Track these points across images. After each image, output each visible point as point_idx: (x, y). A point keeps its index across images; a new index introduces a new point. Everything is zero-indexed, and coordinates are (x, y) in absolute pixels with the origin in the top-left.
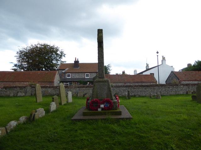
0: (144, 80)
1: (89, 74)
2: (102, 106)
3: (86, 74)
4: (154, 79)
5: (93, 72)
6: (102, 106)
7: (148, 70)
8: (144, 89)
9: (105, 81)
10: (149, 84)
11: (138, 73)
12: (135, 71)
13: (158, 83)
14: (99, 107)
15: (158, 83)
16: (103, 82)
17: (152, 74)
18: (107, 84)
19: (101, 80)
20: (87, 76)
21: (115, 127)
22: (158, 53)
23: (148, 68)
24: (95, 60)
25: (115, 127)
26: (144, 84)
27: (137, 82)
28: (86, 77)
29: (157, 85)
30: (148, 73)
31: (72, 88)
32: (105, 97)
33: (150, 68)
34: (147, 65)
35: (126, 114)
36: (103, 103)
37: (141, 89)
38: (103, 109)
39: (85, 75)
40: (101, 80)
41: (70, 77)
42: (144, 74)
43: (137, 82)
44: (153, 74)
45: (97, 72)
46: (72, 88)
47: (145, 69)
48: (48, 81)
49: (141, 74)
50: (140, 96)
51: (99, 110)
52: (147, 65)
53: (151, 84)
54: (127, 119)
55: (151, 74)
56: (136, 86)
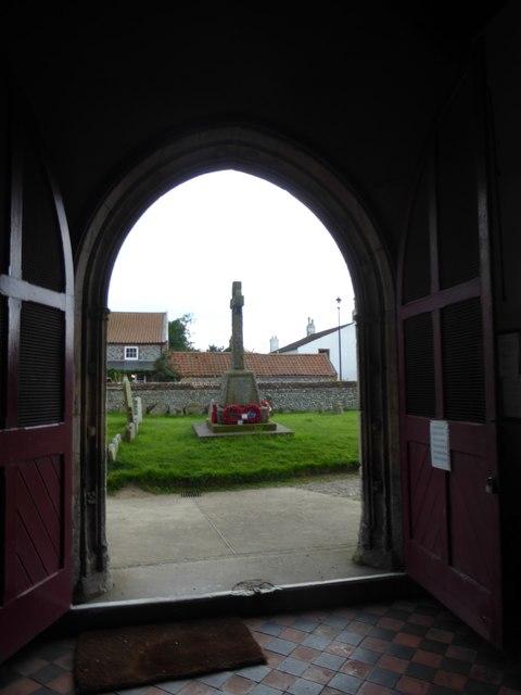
0: (302, 370)
1: (136, 347)
2: (245, 416)
3: (126, 348)
4: (328, 365)
5: (151, 344)
6: (245, 416)
7: (312, 337)
8: (303, 393)
9: (247, 375)
10: (315, 381)
11: (281, 346)
12: (273, 340)
13: (338, 379)
14: (240, 418)
15: (338, 379)
16: (243, 376)
17: (325, 352)
18: (249, 379)
19: (240, 372)
20: (131, 353)
21: (272, 442)
22: (339, 300)
23: (312, 331)
24: (223, 343)
25: (272, 442)
26: (302, 381)
27: (284, 376)
28: (126, 359)
29: (335, 385)
30: (311, 348)
31: (113, 390)
32: (246, 401)
33: (317, 331)
34: (311, 325)
35: (281, 429)
36: (245, 412)
37: (296, 394)
38: (245, 421)
39: (122, 351)
40: (240, 372)
41: (137, 359)
42: (302, 350)
43: (284, 376)
44: (327, 351)
45: (162, 344)
46: (113, 390)
47: (304, 335)
48: (240, 379)
49: (287, 353)
50: (293, 411)
51: (240, 423)
52: (311, 325)
53: (322, 381)
54: (287, 434)
55: (321, 351)
56: (283, 385)
